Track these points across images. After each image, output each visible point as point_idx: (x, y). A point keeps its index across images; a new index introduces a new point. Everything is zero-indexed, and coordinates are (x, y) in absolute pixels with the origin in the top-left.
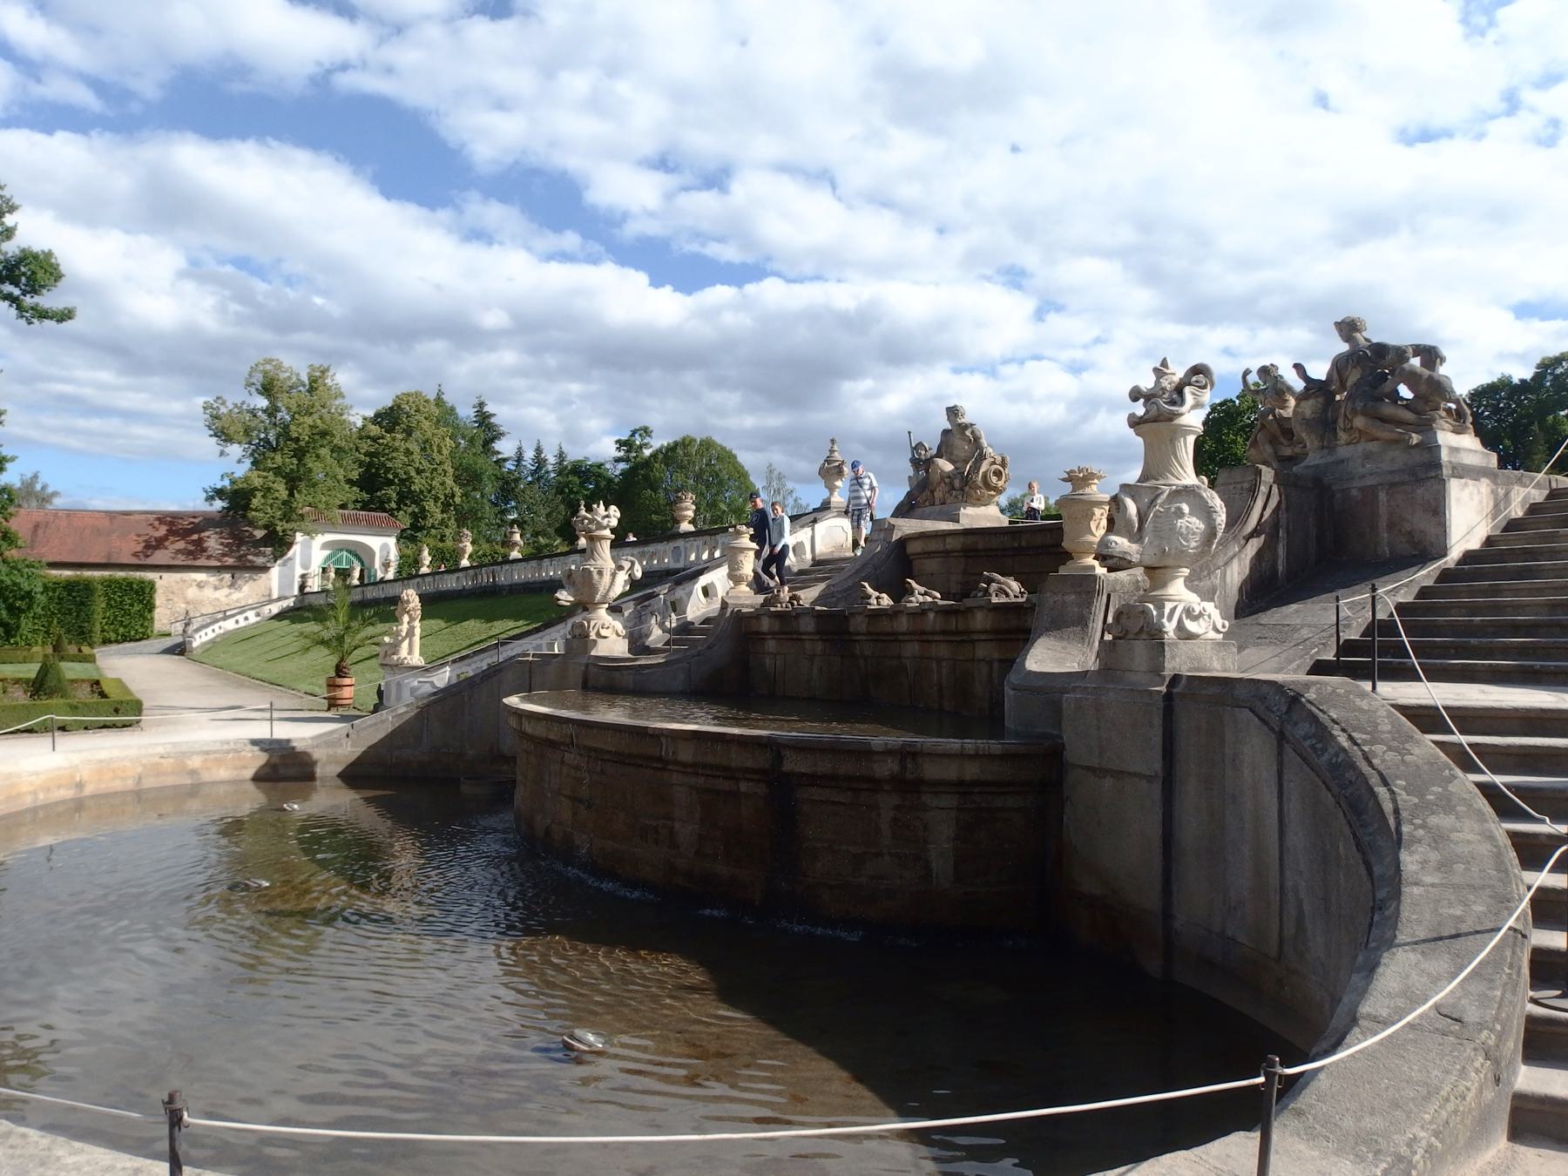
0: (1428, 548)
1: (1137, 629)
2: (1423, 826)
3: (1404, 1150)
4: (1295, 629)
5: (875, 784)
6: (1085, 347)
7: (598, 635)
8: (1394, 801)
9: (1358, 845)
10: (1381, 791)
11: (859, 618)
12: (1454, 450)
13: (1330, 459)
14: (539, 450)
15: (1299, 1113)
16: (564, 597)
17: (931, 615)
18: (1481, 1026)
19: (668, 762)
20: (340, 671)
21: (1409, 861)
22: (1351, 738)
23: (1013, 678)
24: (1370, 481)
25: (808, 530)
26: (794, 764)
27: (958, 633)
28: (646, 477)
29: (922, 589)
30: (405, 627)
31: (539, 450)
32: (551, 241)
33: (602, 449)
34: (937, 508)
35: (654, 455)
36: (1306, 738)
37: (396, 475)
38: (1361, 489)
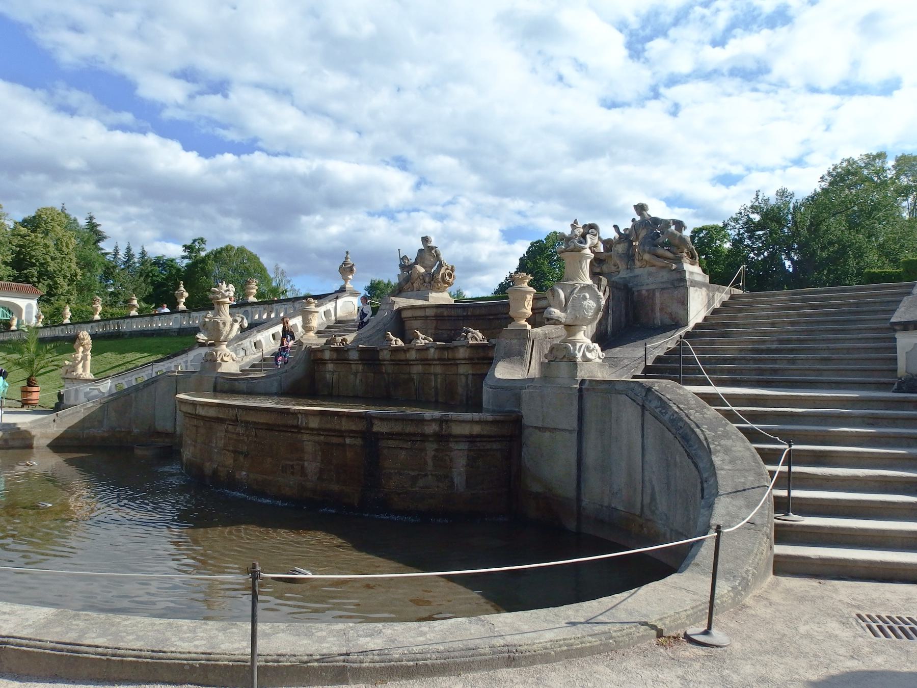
0: (678, 322)
1: (561, 356)
2: (719, 445)
3: (744, 575)
4: (621, 360)
5: (424, 437)
6: (444, 206)
7: (222, 360)
8: (704, 435)
9: (689, 456)
10: (697, 430)
11: (385, 352)
12: (691, 273)
13: (632, 275)
14: (129, 249)
15: (697, 565)
16: (202, 337)
17: (432, 350)
18: (763, 525)
19: (301, 429)
20: (30, 382)
21: (717, 460)
22: (678, 407)
23: (488, 380)
24: (651, 287)
25: (333, 303)
26: (378, 427)
27: (449, 359)
28: (203, 269)
29: (423, 336)
30: (80, 355)
31: (129, 249)
32: (114, 117)
33: (174, 251)
34: (415, 293)
35: (208, 256)
36: (656, 408)
37: (37, 260)
38: (648, 291)
